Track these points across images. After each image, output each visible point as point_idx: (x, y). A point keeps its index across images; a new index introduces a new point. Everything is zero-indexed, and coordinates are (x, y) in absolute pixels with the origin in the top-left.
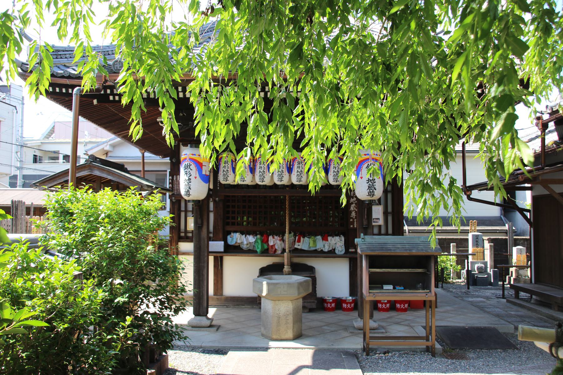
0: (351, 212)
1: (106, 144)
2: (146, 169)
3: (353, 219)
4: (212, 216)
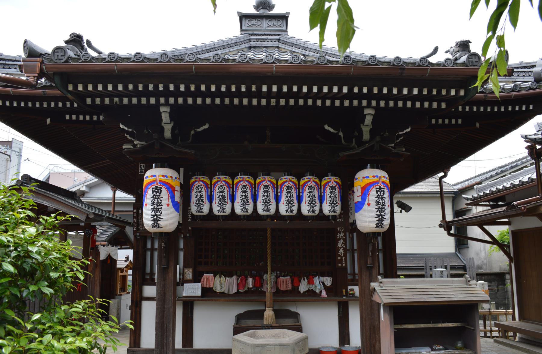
0: (338, 249)
1: (82, 185)
2: (116, 210)
3: (342, 257)
4: (181, 255)
